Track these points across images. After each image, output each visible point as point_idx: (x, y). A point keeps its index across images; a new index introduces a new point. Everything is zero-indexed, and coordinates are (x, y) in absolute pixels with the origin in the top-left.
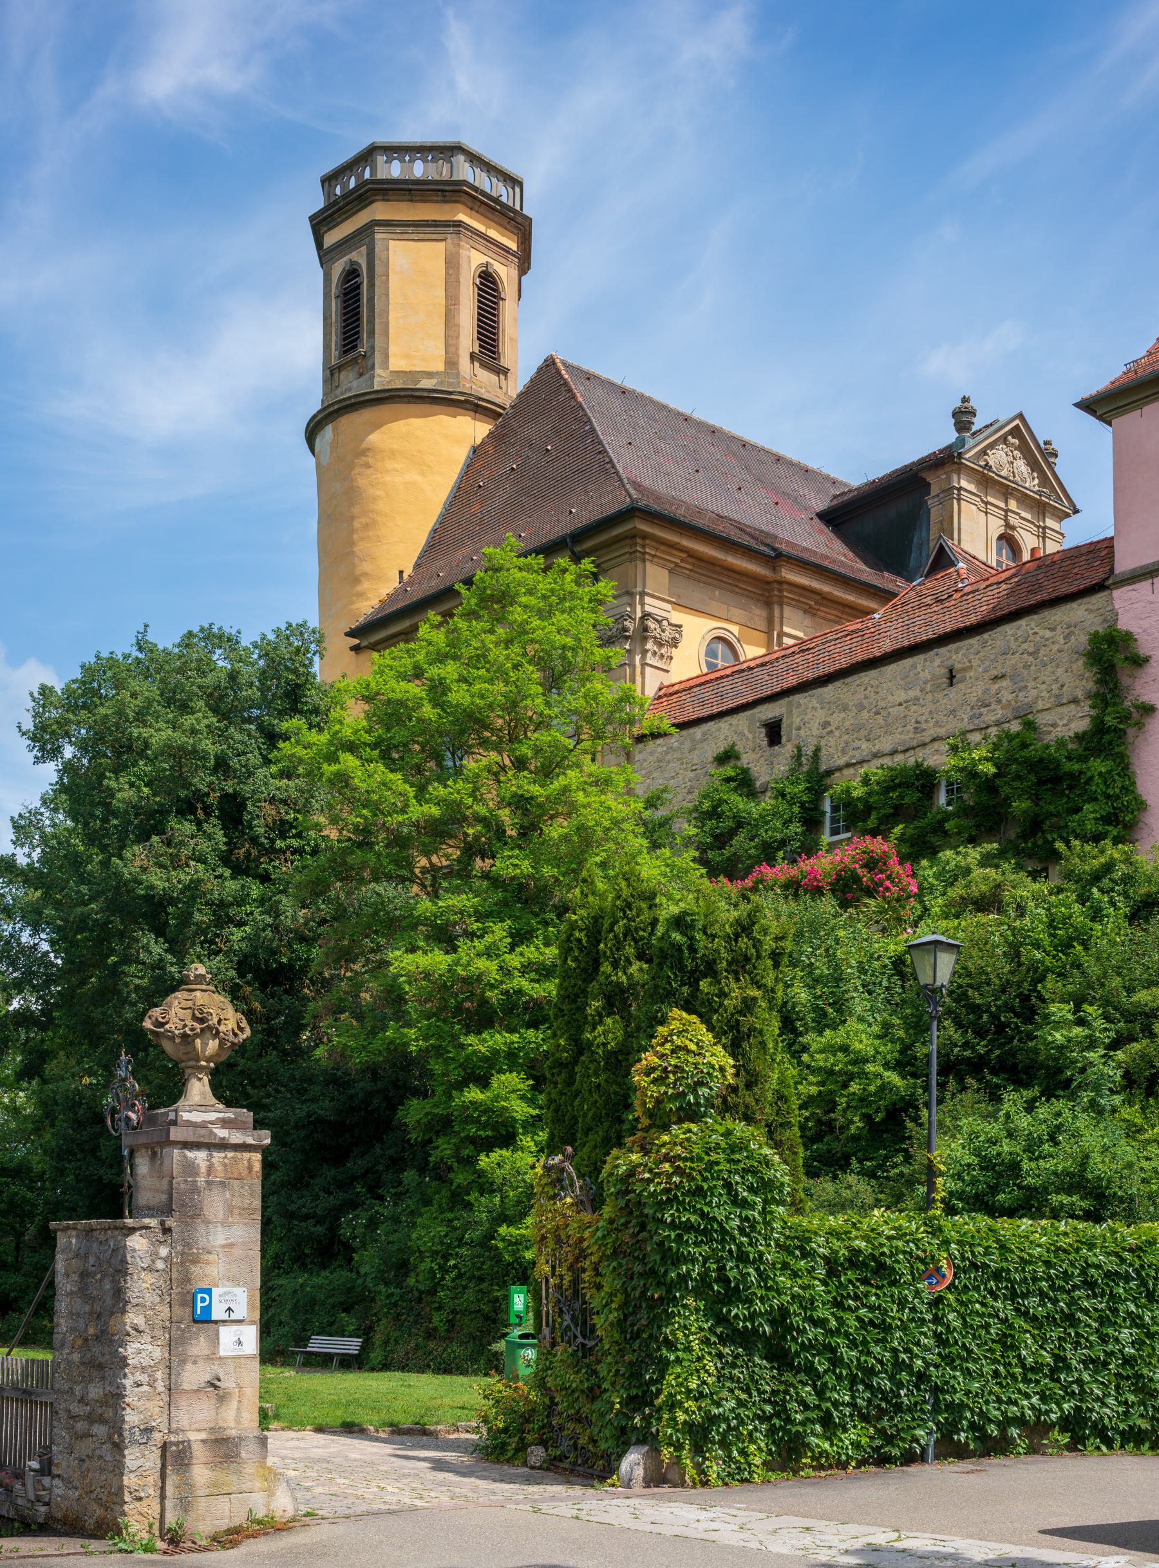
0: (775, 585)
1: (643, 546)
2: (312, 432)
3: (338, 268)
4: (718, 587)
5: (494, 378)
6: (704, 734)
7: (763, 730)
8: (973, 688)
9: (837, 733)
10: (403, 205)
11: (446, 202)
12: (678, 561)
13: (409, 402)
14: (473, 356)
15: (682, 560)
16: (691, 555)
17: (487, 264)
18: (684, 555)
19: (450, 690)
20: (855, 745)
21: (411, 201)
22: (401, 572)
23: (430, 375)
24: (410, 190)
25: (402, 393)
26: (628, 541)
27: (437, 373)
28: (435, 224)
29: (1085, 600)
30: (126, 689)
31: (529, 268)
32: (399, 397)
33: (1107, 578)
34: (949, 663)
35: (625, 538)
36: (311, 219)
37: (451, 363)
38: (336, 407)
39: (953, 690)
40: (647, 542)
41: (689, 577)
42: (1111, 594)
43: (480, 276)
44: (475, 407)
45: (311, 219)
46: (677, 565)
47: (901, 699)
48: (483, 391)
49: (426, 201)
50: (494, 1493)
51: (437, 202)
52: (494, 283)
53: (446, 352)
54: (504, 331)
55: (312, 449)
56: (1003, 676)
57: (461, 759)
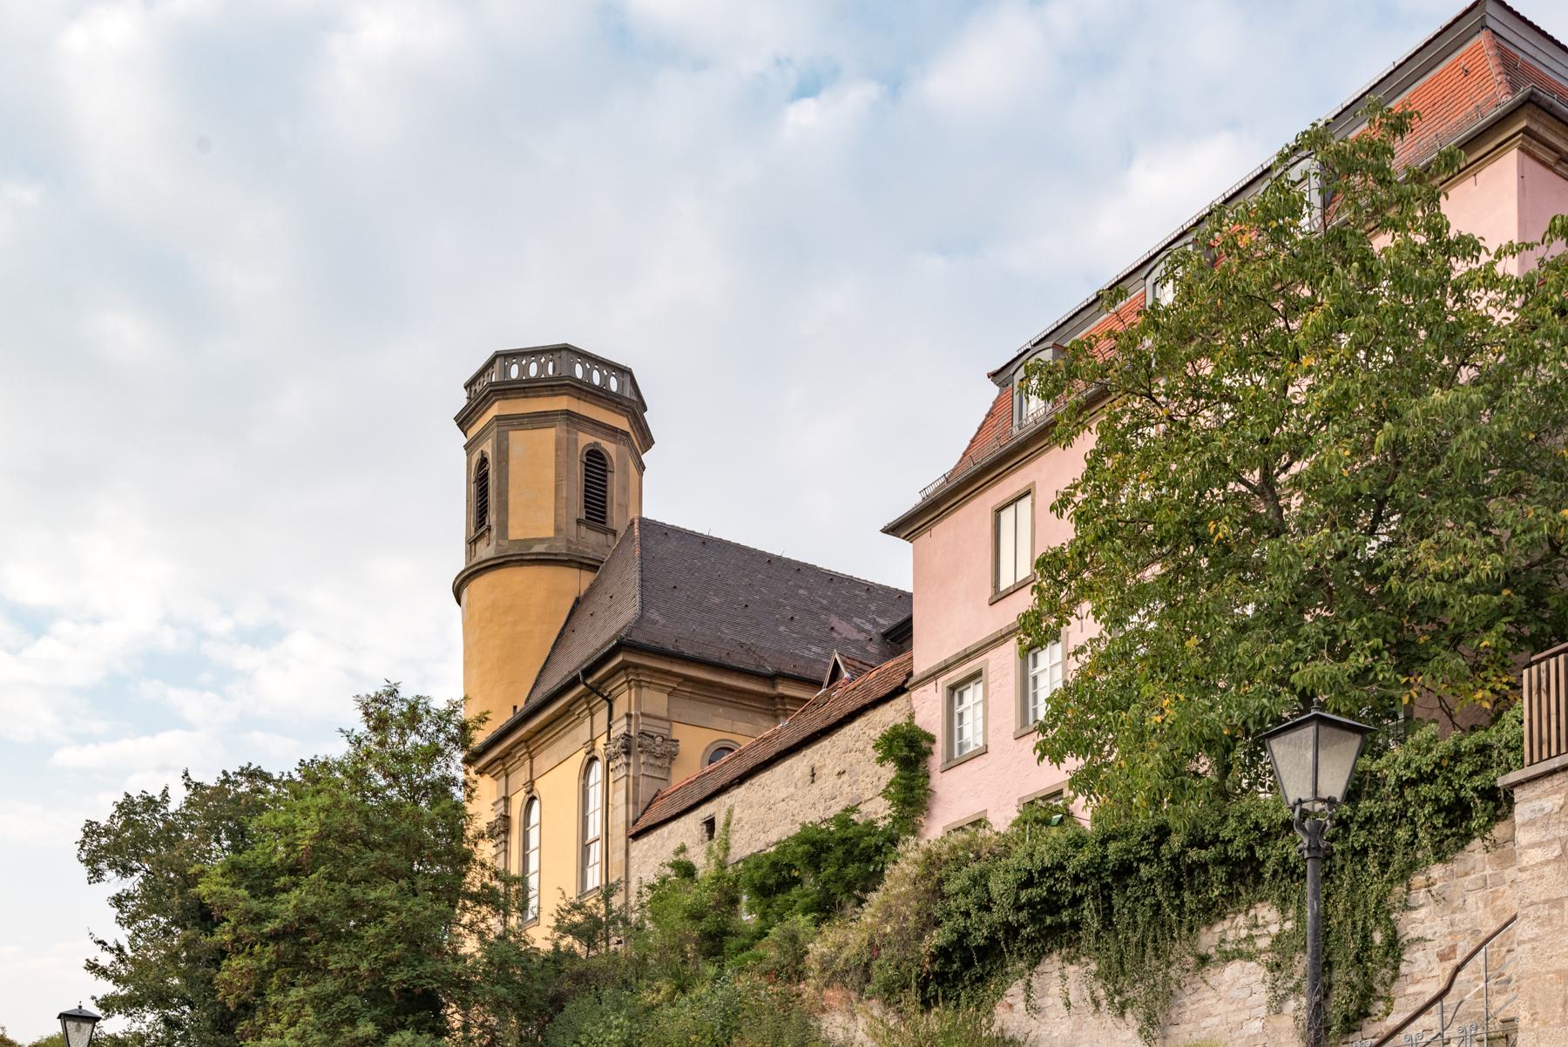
0: (777, 700)
1: (638, 675)
3: (476, 457)
4: (721, 705)
5: (602, 537)
6: (669, 833)
7: (705, 827)
8: (827, 781)
9: (746, 828)
10: (547, 399)
11: (556, 395)
12: (675, 685)
13: (522, 565)
14: (579, 522)
16: (687, 679)
17: (596, 443)
18: (681, 680)
19: (1431, 784)
20: (756, 837)
21: (526, 397)
22: (515, 707)
23: (541, 541)
24: (524, 388)
25: (514, 558)
26: (622, 672)
27: (548, 539)
28: (545, 414)
29: (893, 702)
31: (644, 468)
32: (512, 561)
33: (906, 681)
34: (811, 763)
38: (534, 557)
39: (814, 785)
40: (640, 671)
41: (690, 698)
42: (909, 701)
43: (588, 454)
46: (675, 689)
47: (783, 796)
48: (590, 550)
49: (539, 396)
51: (548, 396)
52: (603, 458)
53: (555, 521)
54: (612, 498)
55: (459, 602)
56: (844, 772)
57: (110, 866)
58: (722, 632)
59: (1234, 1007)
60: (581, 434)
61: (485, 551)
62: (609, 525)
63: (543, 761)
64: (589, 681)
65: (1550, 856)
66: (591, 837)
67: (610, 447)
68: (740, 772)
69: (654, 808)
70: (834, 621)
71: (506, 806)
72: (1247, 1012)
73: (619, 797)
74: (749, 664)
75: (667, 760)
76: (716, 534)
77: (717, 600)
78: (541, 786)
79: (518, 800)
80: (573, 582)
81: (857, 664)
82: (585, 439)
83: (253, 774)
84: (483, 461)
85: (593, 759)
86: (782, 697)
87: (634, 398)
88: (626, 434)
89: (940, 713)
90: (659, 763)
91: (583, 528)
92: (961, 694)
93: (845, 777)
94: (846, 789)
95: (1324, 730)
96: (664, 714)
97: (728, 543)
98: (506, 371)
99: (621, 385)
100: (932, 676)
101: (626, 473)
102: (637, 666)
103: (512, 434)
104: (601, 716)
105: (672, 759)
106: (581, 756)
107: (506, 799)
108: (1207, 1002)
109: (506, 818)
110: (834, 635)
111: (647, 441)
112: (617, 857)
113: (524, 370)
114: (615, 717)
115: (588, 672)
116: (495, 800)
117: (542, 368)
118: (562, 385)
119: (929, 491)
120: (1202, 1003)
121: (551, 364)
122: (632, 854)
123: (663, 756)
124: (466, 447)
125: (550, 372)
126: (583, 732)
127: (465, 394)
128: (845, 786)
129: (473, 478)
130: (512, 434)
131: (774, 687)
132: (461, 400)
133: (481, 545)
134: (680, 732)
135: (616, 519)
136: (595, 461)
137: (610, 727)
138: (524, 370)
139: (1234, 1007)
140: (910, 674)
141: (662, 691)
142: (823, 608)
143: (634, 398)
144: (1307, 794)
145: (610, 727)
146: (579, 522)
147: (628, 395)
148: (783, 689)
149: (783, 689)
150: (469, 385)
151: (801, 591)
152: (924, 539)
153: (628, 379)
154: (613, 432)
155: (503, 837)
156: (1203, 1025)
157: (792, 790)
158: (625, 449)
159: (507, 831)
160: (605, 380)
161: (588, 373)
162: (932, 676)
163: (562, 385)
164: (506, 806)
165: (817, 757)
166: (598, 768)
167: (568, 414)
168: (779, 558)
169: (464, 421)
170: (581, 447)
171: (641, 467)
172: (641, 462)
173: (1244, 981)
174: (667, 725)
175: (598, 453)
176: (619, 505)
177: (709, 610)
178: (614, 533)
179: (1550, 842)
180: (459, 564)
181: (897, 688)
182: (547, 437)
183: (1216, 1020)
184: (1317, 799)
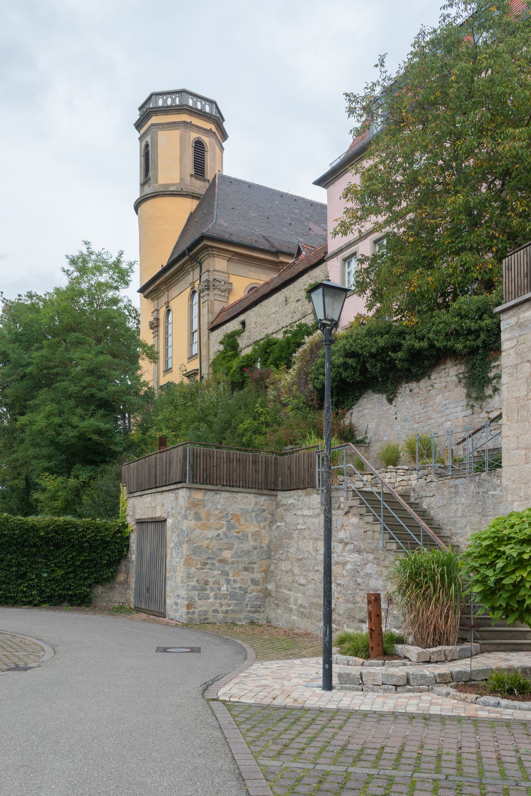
2: (137, 206)
3: (144, 144)
14: (191, 175)
15: (191, 264)
16: (236, 254)
17: (199, 138)
23: (173, 185)
26: (205, 250)
28: (175, 123)
30: (468, 202)
31: (223, 149)
35: (203, 250)
36: (135, 125)
37: (182, 179)
43: (195, 142)
44: (193, 196)
45: (135, 125)
47: (274, 311)
50: (328, 407)
52: (203, 145)
55: (137, 213)
58: (255, 230)
59: (440, 415)
60: (192, 133)
61: (148, 190)
62: (206, 177)
63: (174, 292)
64: (191, 254)
65: (513, 345)
66: (194, 329)
67: (206, 139)
68: (255, 299)
69: (221, 315)
70: (312, 225)
71: (158, 314)
72: (445, 417)
73: (204, 311)
74: (267, 247)
75: (227, 293)
76: (256, 182)
77: (254, 215)
78: (172, 304)
79: (163, 311)
80: (191, 205)
81: (309, 247)
82: (194, 135)
83: (30, 296)
84: (147, 146)
85: (194, 292)
86: (282, 263)
87: (218, 115)
88: (214, 133)
89: (339, 272)
90: (223, 294)
91: (193, 179)
92: (349, 263)
93: (300, 303)
94: (300, 309)
95: (325, 289)
96: (226, 270)
97: (262, 187)
98: (157, 102)
99: (211, 109)
100: (336, 254)
101: (214, 152)
102: (212, 247)
103: (160, 133)
104: (197, 271)
105: (229, 293)
106: (188, 291)
107: (157, 310)
108: (429, 413)
109: (157, 319)
110: (311, 232)
111: (224, 136)
112: (204, 339)
113: (165, 101)
114: (203, 272)
115: (190, 249)
116: (153, 310)
117: (173, 100)
118: (182, 109)
119: (334, 165)
120: (428, 413)
121: (178, 99)
122: (211, 338)
123: (224, 291)
124: (140, 139)
125: (177, 103)
126: (189, 278)
127: (138, 112)
128: (300, 307)
129: (142, 154)
130: (160, 133)
131: (278, 257)
132: (136, 116)
133: (146, 187)
134: (233, 279)
135: (209, 175)
136: (199, 146)
137: (201, 276)
138: (165, 101)
139: (440, 415)
140: (326, 253)
141: (224, 259)
142: (307, 219)
143: (218, 115)
144: (322, 317)
145: (201, 276)
146: (191, 175)
147: (214, 114)
148: (282, 259)
149: (282, 259)
150: (140, 109)
151: (296, 211)
152: (332, 188)
153: (214, 106)
154: (208, 132)
155: (156, 329)
156: (428, 423)
157: (277, 308)
158: (213, 140)
159: (158, 326)
160: (203, 106)
161: (195, 103)
162: (336, 254)
163: (182, 109)
164: (158, 314)
165: (288, 293)
166: (197, 295)
167: (185, 122)
168: (287, 194)
169: (138, 125)
170: (192, 140)
171: (222, 149)
172: (222, 147)
173: (445, 402)
174: (227, 275)
175: (201, 142)
176: (211, 167)
177: (249, 220)
178: (208, 181)
179: (513, 339)
180: (136, 195)
181: (321, 260)
182: (175, 134)
183: (433, 421)
184: (326, 319)
